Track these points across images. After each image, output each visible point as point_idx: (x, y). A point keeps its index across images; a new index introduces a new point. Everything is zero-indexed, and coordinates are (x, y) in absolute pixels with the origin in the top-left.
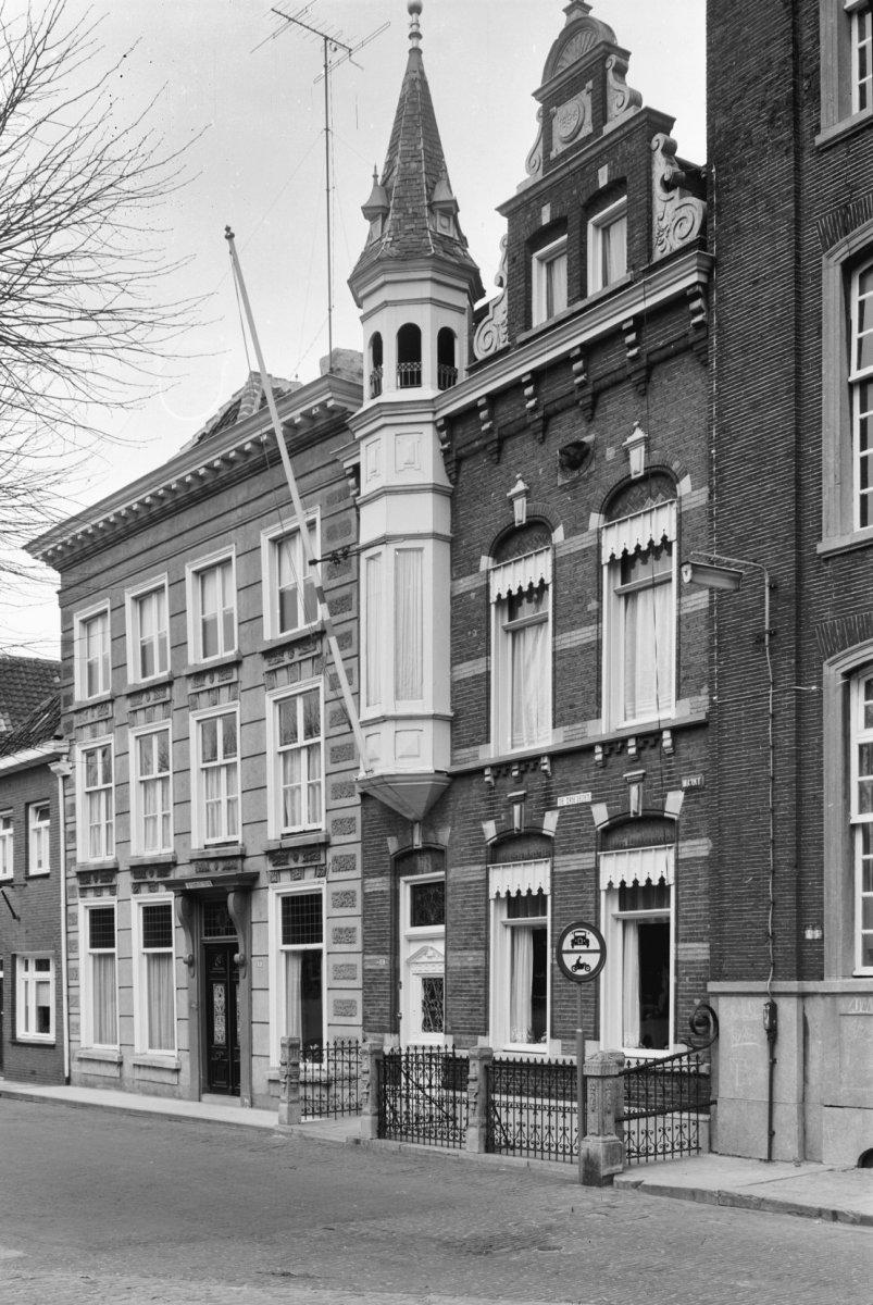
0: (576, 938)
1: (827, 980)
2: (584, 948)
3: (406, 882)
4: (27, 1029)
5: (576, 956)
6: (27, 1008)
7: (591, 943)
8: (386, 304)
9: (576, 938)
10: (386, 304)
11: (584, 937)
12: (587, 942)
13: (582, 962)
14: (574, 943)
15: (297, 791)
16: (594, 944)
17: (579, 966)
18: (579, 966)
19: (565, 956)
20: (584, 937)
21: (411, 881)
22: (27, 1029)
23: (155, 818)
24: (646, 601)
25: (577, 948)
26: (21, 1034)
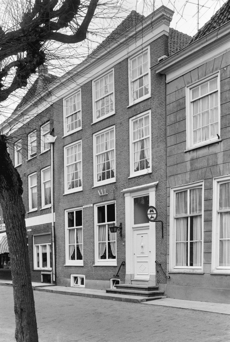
0: (151, 210)
1: (111, 233)
2: (152, 213)
3: (96, 206)
4: (38, 266)
5: (151, 215)
6: (225, 223)
7: (154, 212)
8: (101, 14)
9: (151, 210)
10: (101, 14)
11: (152, 210)
12: (153, 212)
13: (152, 216)
14: (150, 212)
15: (215, 111)
16: (155, 212)
17: (152, 217)
18: (152, 217)
19: (148, 215)
20: (152, 210)
21: (97, 206)
22: (38, 266)
23: (207, 112)
24: (34, 180)
25: (151, 213)
26: (36, 268)
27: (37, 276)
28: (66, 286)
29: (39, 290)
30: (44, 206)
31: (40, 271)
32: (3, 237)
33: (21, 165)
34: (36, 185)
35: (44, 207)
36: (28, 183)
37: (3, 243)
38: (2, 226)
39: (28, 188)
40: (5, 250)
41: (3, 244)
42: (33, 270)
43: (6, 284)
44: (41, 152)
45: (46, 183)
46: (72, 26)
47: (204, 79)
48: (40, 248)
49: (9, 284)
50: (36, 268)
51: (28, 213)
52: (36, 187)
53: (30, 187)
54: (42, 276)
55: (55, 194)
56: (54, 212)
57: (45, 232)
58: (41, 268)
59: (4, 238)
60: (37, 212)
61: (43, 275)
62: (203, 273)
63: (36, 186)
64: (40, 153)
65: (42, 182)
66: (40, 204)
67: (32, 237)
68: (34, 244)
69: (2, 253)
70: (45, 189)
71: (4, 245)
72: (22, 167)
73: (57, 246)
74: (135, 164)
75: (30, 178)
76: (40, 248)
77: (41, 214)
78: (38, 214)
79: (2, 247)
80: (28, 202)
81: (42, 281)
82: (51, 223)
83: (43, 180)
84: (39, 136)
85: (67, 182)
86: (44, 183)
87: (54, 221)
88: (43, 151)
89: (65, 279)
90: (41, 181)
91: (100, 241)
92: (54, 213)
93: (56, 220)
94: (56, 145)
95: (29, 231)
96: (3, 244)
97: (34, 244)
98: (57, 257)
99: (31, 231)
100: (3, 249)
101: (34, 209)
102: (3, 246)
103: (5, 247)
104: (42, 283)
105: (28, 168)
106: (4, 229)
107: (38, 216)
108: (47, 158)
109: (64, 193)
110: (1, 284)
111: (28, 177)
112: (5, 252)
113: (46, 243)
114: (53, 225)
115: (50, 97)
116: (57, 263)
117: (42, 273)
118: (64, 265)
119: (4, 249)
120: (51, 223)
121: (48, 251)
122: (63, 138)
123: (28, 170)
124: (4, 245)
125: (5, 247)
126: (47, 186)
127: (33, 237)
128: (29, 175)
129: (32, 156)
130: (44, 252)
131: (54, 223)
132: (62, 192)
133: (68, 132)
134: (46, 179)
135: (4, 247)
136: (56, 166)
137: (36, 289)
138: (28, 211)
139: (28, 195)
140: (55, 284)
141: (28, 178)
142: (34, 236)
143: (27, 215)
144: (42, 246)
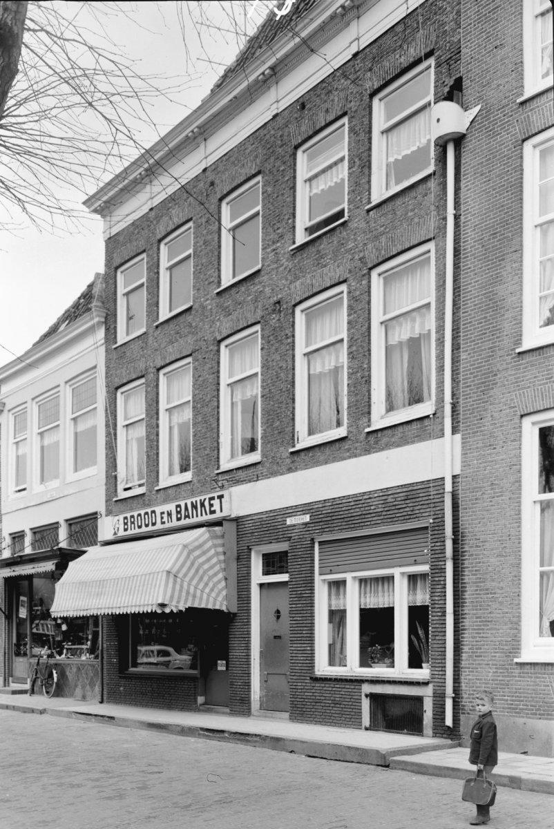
3: (534, 424)
26: (323, 668)
27: (336, 703)
28: (525, 753)
29: (415, 768)
30: (382, 417)
31: (360, 681)
32: (185, 546)
33: (259, 271)
34: (143, 416)
35: (380, 418)
36: (293, 336)
37: (184, 570)
38: (153, 512)
39: (294, 356)
40: (190, 598)
41: (185, 575)
42: (311, 678)
43: (202, 729)
44: (223, 282)
45: (390, 323)
47: (51, 395)
48: (352, 588)
49: (223, 731)
50: (323, 668)
51: (292, 453)
52: (187, 406)
53: (301, 348)
54: (366, 704)
55: (463, 356)
56: (455, 430)
57: (392, 520)
58: (352, 666)
59: (185, 553)
60: (346, 445)
61: (373, 697)
63: (143, 419)
64: (369, 202)
65: (377, 316)
66: (361, 407)
67: (313, 547)
68: (320, 574)
69: (181, 608)
70: (309, 375)
71: (187, 579)
72: (264, 278)
73: (468, 578)
74: (396, 356)
75: (304, 316)
76: (352, 588)
77: (367, 451)
78: (349, 450)
79: (182, 586)
80: (294, 408)
81: (366, 720)
82: (443, 479)
83: (166, 403)
84: (362, 136)
85: (538, 294)
86: (166, 410)
87: (457, 472)
88: (379, 193)
89: (521, 721)
90: (369, 314)
91: (546, 562)
92: (458, 437)
93: (465, 464)
94: (469, 146)
95: (294, 522)
96: (185, 575)
97: (320, 574)
98: (467, 623)
99: (306, 524)
100: (184, 594)
101: (312, 437)
102: (182, 581)
103: (189, 588)
104: (367, 729)
105: (297, 278)
106: (163, 523)
107: (350, 457)
108: (410, 214)
109: (518, 342)
110: (179, 729)
111: (293, 313)
112: (189, 605)
113: (393, 567)
114: (448, 487)
115: (202, 146)
116: (466, 649)
117: (367, 689)
118: (516, 660)
119: (188, 593)
120: (443, 479)
121: (400, 600)
122: (522, 103)
123: (298, 283)
124: (187, 579)
125: (189, 588)
126: (324, 364)
127: (317, 546)
128: (300, 302)
129: (310, 230)
130: (376, 601)
131: (454, 477)
132: (507, 342)
133: (543, 77)
134: (318, 339)
135: (185, 584)
136: (469, 235)
137: (395, 762)
138: (294, 446)
139: (294, 382)
140: (449, 742)
141: (294, 318)
142: (321, 543)
143: (288, 461)
144: (363, 581)
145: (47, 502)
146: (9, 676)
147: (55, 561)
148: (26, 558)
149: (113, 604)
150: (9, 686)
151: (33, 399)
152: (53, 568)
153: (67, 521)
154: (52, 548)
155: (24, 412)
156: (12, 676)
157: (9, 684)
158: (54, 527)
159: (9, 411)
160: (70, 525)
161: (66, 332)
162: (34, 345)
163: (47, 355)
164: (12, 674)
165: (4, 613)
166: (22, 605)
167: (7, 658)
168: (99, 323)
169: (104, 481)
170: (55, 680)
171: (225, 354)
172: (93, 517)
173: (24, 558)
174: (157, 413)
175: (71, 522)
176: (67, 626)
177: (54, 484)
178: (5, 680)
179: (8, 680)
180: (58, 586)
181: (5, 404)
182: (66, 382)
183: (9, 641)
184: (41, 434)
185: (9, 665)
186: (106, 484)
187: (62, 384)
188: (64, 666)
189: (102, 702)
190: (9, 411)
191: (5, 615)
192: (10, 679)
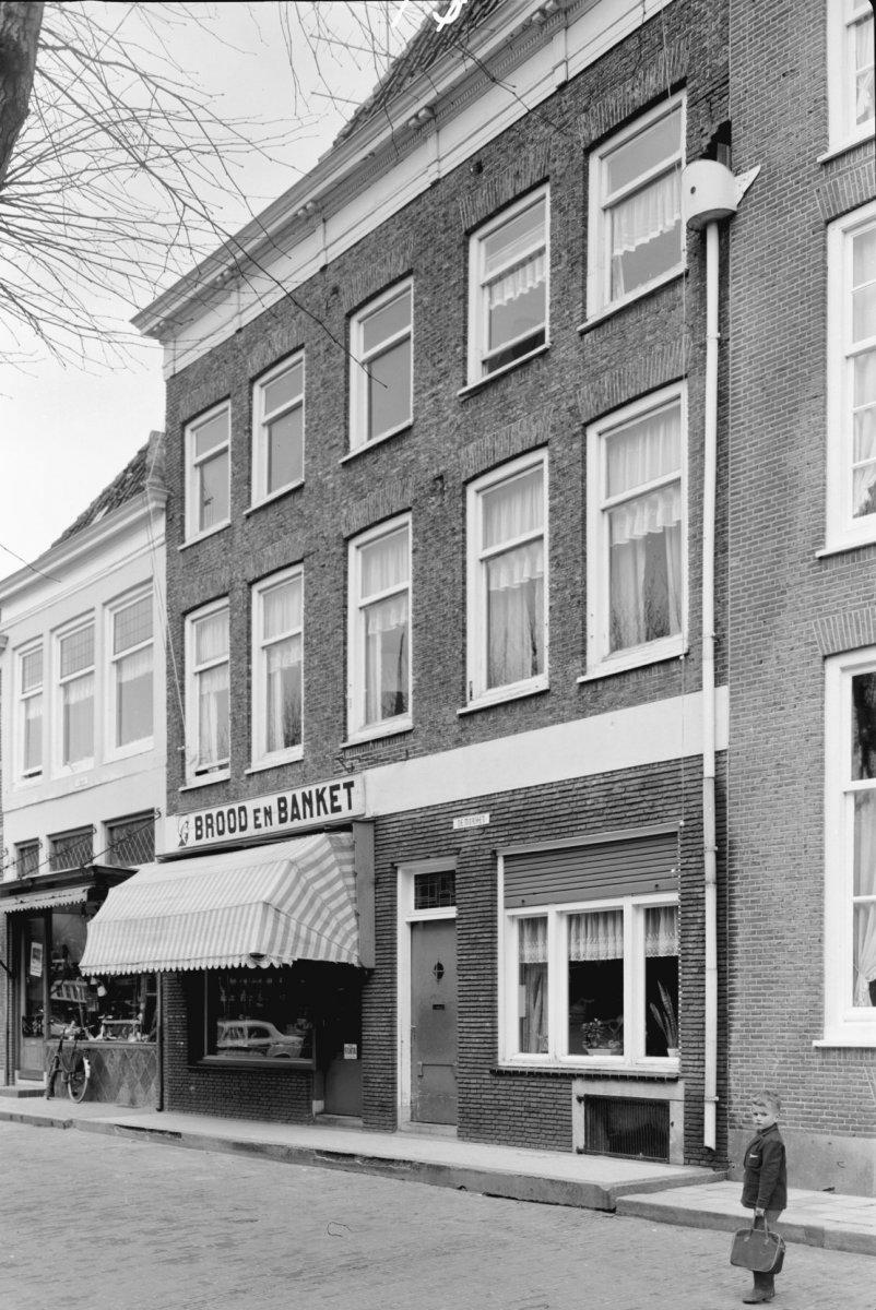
3: (844, 669)
26: (510, 1055)
27: (531, 1111)
28: (830, 1190)
29: (656, 1213)
30: (604, 660)
31: (569, 1077)
32: (293, 863)
33: (409, 429)
34: (227, 657)
35: (601, 661)
36: (464, 531)
37: (291, 901)
38: (243, 809)
39: (464, 563)
40: (301, 945)
41: (293, 909)
42: (492, 1072)
43: (319, 1152)
44: (352, 446)
45: (616, 511)
46: (24, 293)
47: (81, 625)
48: (557, 930)
49: (352, 1156)
50: (510, 1055)
51: (462, 716)
52: (296, 641)
53: (475, 550)
54: (578, 1113)
55: (732, 562)
56: (719, 680)
57: (620, 822)
58: (557, 1053)
59: (293, 874)
60: (548, 703)
61: (590, 1102)
62: (675, 1076)
63: (226, 663)
64: (584, 320)
65: (596, 499)
66: (571, 643)
67: (494, 865)
68: (507, 908)
69: (286, 962)
70: (489, 592)
71: (296, 915)
72: (417, 439)
73: (740, 913)
74: (626, 563)
75: (480, 500)
76: (557, 930)
77: (581, 713)
78: (551, 711)
79: (287, 927)
80: (465, 645)
81: (579, 1138)
82: (700, 756)
83: (262, 636)
84: (573, 215)
85: (851, 465)
86: (263, 648)
87: (723, 745)
88: (599, 304)
89: (823, 1139)
90: (584, 495)
91: (863, 888)
92: (724, 690)
93: (735, 733)
94: (742, 231)
95: (464, 826)
96: (293, 909)
97: (507, 908)
98: (738, 984)
99: (484, 828)
100: (291, 939)
101: (493, 691)
102: (288, 918)
103: (298, 929)
104: (580, 1152)
105: (469, 439)
106: (258, 826)
107: (553, 723)
108: (648, 338)
109: (820, 540)
110: (283, 1151)
111: (464, 495)
112: (298, 955)
113: (622, 896)
114: (709, 769)
115: (320, 231)
116: (736, 1025)
117: (580, 1088)
118: (816, 1043)
119: (297, 937)
120: (700, 756)
121: (633, 948)
122: (826, 163)
123: (471, 447)
124: (296, 915)
125: (298, 929)
126: (512, 575)
127: (501, 863)
128: (475, 477)
129: (490, 364)
130: (595, 949)
131: (718, 754)
132: (801, 541)
133: (859, 122)
134: (503, 536)
135: (293, 923)
136: (742, 371)
137: (625, 1204)
138: (465, 705)
139: (464, 604)
140: (710, 1172)
141: (464, 502)
142: (507, 858)
143: (456, 728)
144: (573, 918)
145: (74, 793)
146: (14, 1069)
147: (88, 887)
148: (42, 882)
149: (178, 955)
150: (14, 1084)
151: (52, 631)
152: (84, 897)
153: (105, 823)
154: (82, 865)
155: (39, 650)
156: (19, 1069)
157: (14, 1080)
158: (86, 832)
159: (14, 649)
160: (111, 829)
161: (104, 525)
162: (53, 546)
163: (74, 561)
164: (19, 1065)
165: (7, 969)
166: (35, 957)
167: (10, 1040)
168: (157, 511)
169: (164, 760)
170: (88, 1074)
171: (356, 559)
172: (147, 817)
173: (37, 882)
174: (249, 653)
175: (113, 825)
176: (106, 989)
177: (85, 765)
178: (8, 1074)
179: (13, 1074)
180: (92, 926)
181: (7, 638)
182: (105, 604)
183: (14, 1013)
184: (65, 686)
185: (14, 1052)
186: (168, 766)
187: (99, 607)
188: (101, 1053)
189: (161, 1110)
190: (14, 649)
191: (8, 971)
192: (17, 1072)
